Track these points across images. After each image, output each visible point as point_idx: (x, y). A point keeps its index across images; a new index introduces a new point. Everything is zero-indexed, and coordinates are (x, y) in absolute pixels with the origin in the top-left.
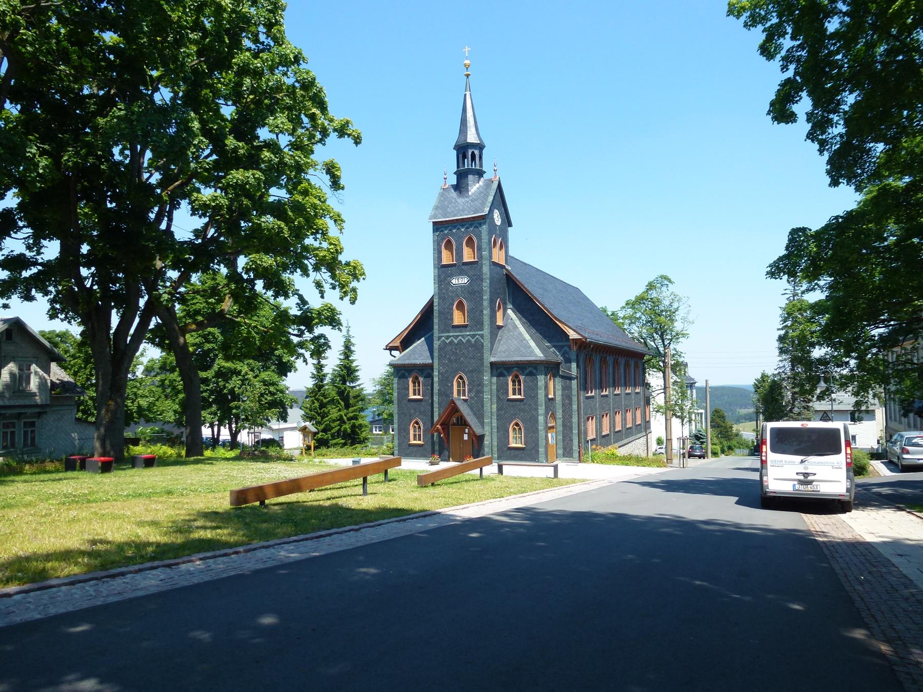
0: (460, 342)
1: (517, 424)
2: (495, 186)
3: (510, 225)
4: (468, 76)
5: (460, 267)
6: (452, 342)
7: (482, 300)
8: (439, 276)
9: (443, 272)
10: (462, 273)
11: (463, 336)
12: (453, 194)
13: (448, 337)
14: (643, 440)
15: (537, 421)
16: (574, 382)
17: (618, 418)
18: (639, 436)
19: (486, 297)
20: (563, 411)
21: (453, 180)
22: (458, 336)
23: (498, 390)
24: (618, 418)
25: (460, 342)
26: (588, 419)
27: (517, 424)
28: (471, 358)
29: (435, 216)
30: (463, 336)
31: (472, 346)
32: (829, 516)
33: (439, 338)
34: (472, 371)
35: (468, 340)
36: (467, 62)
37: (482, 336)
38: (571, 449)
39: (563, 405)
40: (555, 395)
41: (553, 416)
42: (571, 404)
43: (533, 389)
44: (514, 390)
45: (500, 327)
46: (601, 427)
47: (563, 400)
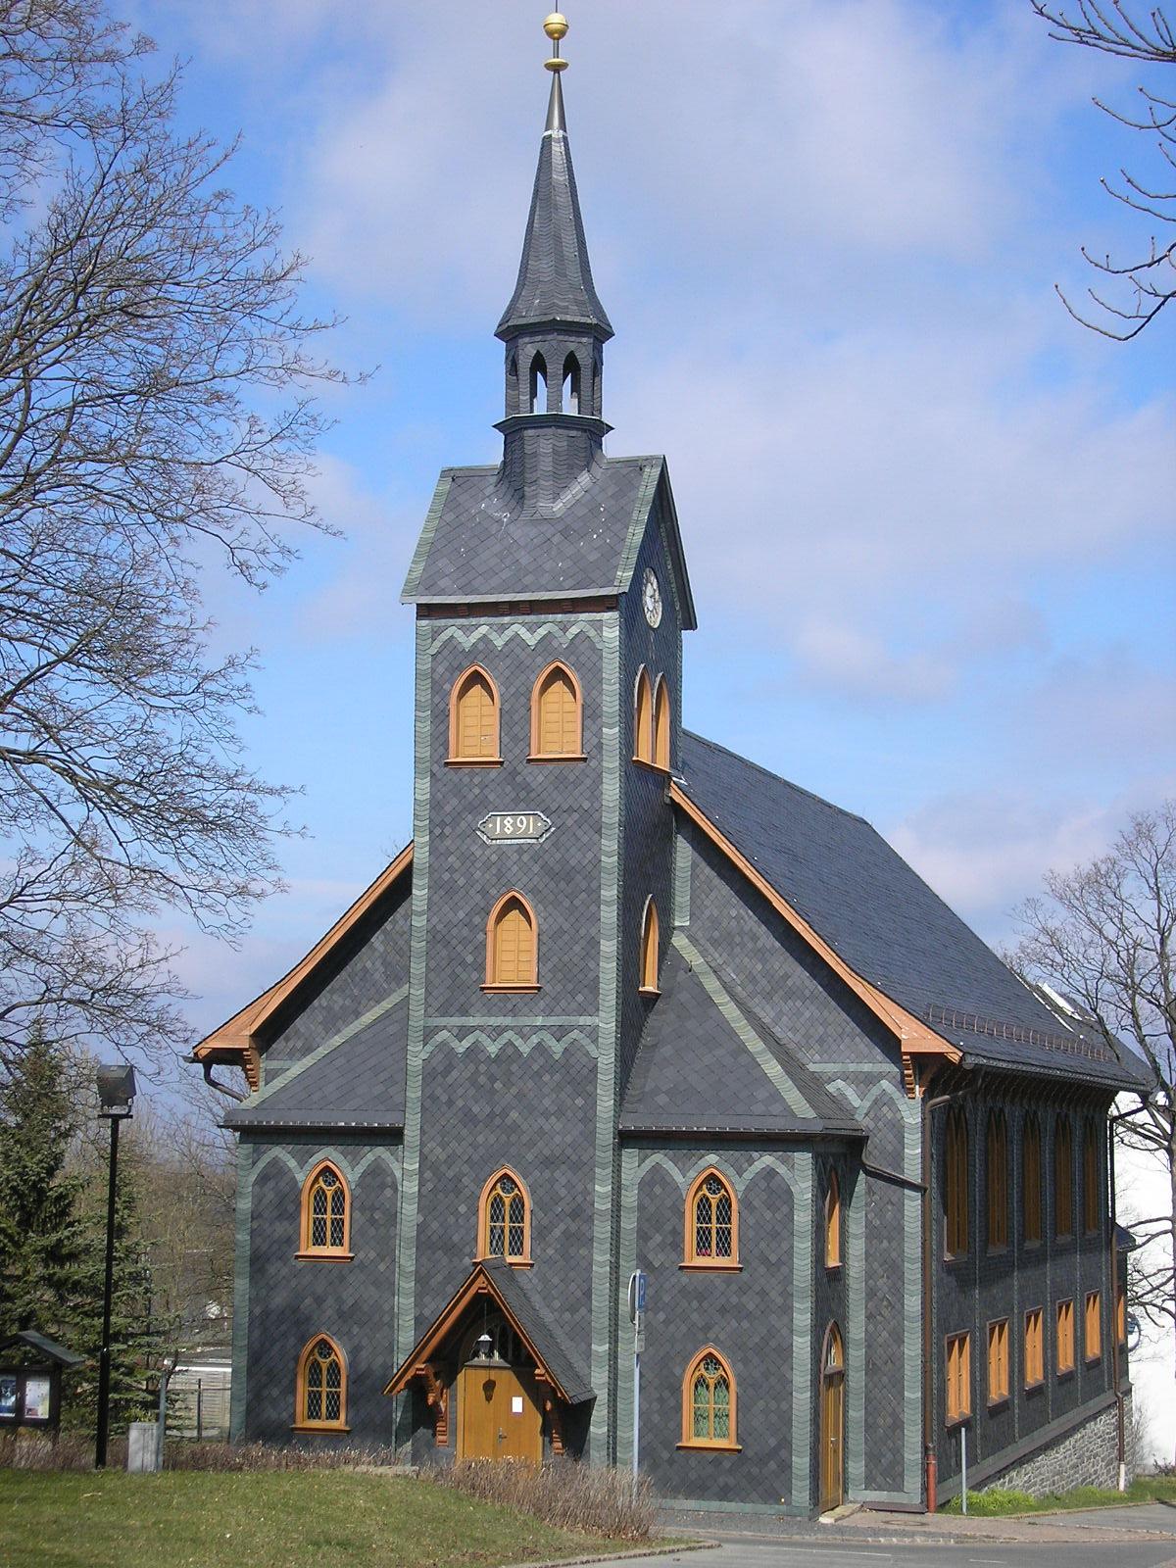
0: (509, 1054)
1: (711, 1360)
2: (648, 489)
3: (690, 623)
4: (557, 68)
5: (515, 776)
6: (474, 1051)
7: (598, 902)
8: (435, 804)
9: (453, 791)
10: (522, 799)
11: (520, 1032)
12: (492, 505)
13: (462, 1032)
14: (1104, 1424)
15: (786, 1352)
16: (913, 1204)
17: (999, 1353)
18: (1094, 1404)
19: (610, 892)
20: (869, 1317)
21: (491, 452)
22: (500, 1030)
23: (643, 1236)
24: (1034, 1340)
25: (509, 1054)
26: (951, 1344)
27: (711, 1360)
28: (546, 1115)
29: (427, 584)
30: (520, 1032)
31: (551, 1066)
32: (533, 1406)
33: (428, 1034)
34: (548, 1163)
35: (540, 1047)
36: (556, 19)
37: (593, 1034)
38: (898, 1460)
39: (871, 1294)
40: (843, 1256)
41: (839, 1333)
42: (898, 1293)
43: (775, 1235)
44: (703, 1237)
45: (651, 1000)
46: (1055, 1357)
47: (869, 1275)
